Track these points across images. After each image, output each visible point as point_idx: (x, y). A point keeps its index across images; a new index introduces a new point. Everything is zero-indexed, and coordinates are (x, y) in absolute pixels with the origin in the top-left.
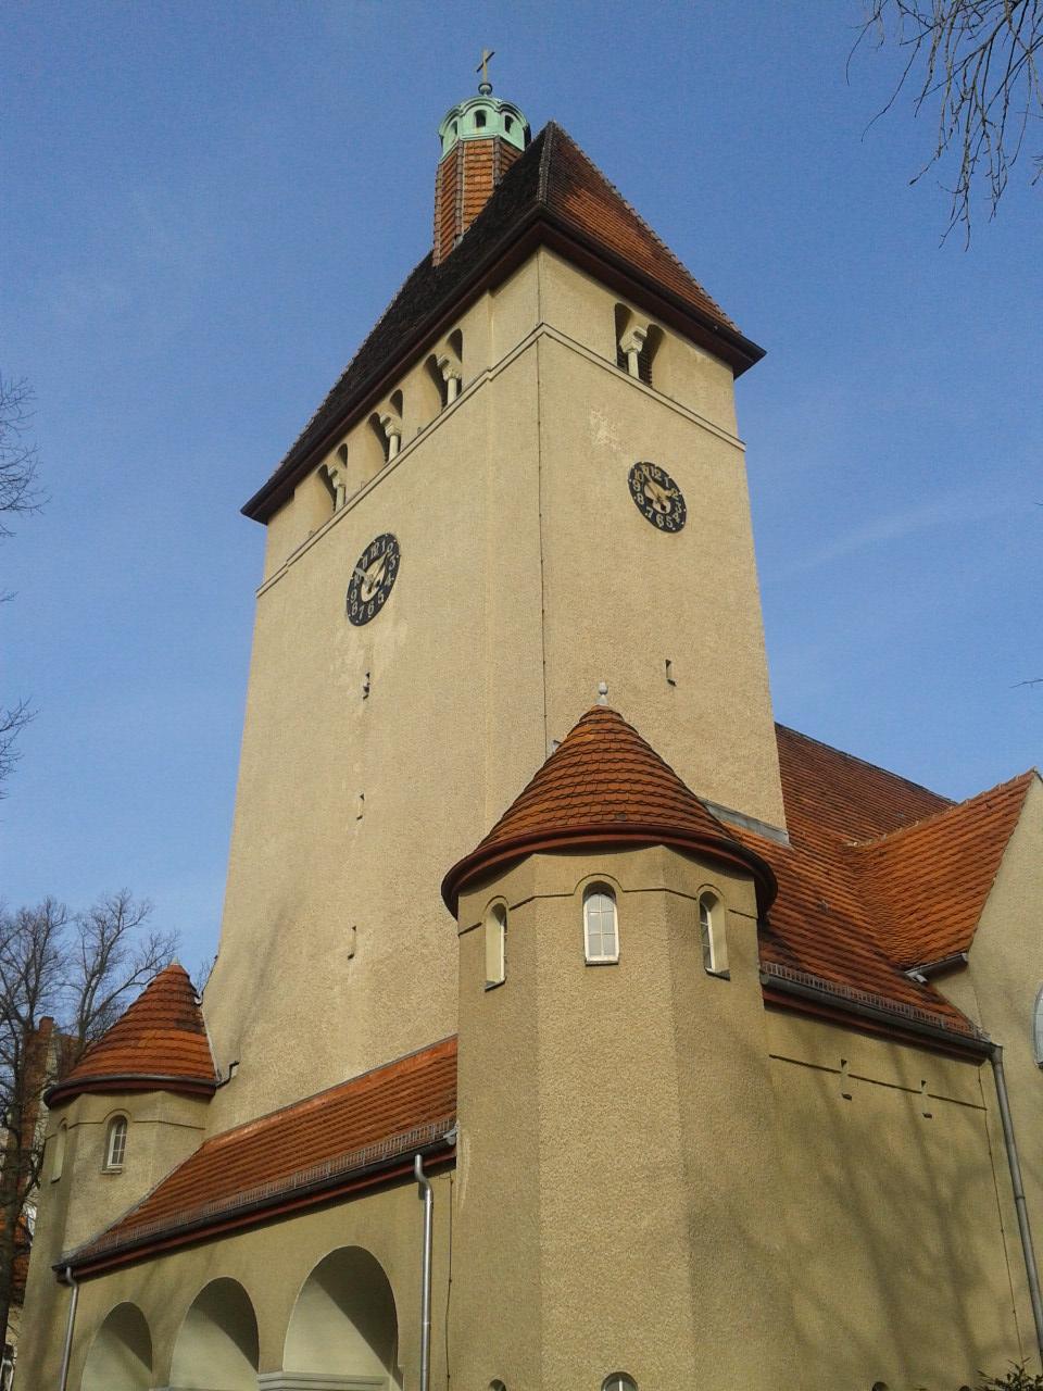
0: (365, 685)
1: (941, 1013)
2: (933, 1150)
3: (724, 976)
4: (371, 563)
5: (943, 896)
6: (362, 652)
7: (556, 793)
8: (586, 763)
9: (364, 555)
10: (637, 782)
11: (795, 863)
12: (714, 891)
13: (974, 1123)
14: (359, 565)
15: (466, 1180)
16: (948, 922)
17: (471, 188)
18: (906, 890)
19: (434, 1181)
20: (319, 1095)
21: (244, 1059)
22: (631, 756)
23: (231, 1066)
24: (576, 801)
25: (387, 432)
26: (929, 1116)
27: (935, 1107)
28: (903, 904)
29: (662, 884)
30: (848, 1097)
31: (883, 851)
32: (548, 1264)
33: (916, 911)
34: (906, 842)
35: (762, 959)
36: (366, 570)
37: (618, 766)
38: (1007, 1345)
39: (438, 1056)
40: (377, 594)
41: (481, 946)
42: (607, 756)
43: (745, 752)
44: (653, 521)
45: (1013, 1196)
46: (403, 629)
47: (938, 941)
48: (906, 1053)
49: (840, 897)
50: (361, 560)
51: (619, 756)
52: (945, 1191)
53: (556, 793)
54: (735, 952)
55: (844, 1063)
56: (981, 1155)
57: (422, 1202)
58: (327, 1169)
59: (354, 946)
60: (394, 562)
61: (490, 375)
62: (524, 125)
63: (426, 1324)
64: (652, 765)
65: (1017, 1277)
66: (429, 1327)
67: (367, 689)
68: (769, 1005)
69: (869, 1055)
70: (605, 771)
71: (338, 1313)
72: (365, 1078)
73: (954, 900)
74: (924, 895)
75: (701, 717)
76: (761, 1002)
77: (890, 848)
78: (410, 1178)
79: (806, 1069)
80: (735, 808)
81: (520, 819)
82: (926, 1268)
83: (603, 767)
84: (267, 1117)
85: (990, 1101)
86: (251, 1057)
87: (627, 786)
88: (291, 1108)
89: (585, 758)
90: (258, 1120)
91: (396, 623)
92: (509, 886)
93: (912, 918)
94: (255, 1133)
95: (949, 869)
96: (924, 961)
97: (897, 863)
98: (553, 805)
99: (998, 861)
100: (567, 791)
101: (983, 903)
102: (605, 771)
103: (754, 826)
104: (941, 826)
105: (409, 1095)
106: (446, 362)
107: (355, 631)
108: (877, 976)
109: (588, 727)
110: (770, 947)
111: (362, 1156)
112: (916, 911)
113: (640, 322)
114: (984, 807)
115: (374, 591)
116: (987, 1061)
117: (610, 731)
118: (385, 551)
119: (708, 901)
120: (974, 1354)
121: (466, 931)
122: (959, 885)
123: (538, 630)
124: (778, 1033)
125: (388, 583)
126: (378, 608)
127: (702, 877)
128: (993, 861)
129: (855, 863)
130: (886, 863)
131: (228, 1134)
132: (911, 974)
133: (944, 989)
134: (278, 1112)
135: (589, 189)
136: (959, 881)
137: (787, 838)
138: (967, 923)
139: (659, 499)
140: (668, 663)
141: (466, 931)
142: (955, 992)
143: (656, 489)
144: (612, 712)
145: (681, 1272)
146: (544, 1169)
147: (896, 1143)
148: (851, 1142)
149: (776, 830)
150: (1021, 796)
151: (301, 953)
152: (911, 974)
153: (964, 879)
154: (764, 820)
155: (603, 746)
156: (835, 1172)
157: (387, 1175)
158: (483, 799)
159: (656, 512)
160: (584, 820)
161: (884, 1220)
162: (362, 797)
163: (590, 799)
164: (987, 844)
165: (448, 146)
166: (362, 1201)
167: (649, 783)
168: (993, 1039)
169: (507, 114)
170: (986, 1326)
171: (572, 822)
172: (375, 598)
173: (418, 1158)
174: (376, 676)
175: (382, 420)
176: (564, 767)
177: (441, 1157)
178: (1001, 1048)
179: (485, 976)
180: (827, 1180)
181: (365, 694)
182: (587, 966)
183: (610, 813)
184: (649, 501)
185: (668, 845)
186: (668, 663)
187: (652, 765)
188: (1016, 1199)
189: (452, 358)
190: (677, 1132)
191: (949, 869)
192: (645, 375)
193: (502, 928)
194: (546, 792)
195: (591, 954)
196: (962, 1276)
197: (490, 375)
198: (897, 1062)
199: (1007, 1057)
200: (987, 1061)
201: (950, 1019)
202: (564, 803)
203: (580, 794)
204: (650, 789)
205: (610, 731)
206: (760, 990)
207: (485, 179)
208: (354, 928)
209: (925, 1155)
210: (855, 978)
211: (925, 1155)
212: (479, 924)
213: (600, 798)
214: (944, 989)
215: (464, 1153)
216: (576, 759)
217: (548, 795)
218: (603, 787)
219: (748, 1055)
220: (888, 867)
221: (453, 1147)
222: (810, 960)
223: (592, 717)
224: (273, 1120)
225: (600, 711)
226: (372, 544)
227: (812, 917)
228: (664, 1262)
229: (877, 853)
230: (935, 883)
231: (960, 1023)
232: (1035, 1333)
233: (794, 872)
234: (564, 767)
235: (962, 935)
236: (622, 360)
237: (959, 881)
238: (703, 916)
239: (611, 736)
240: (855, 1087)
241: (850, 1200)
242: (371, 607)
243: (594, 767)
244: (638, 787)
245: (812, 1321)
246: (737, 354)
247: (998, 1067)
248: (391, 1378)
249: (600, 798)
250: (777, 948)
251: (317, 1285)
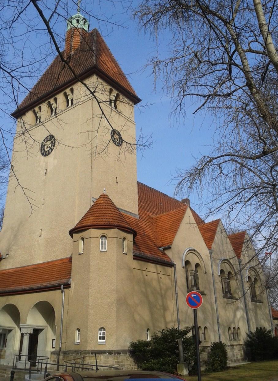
0: (46, 172)
1: (165, 257)
2: (161, 284)
3: (126, 254)
4: (47, 141)
5: (168, 232)
6: (45, 163)
7: (96, 215)
8: (101, 208)
9: (46, 138)
10: (112, 214)
11: (140, 223)
12: (126, 237)
13: (169, 279)
14: (44, 140)
15: (73, 291)
16: (169, 238)
17: (75, 41)
18: (161, 229)
19: (65, 290)
20: (31, 265)
21: (9, 254)
22: (110, 207)
23: (6, 255)
24: (100, 217)
25: (52, 107)
26: (161, 278)
27: (163, 276)
28: (160, 232)
29: (116, 236)
30: (147, 275)
31: (157, 219)
32: (90, 308)
33: (162, 234)
34: (162, 217)
35: (133, 249)
36: (46, 142)
37: (108, 210)
38: (172, 321)
39: (62, 262)
40: (49, 150)
41: (78, 244)
42: (106, 207)
43: (131, 198)
44: (115, 144)
45: (175, 293)
46: (56, 161)
47: (166, 242)
48: (158, 266)
49: (149, 232)
50: (45, 139)
51: (108, 207)
52: (163, 292)
53: (96, 215)
54: (129, 249)
55: (146, 269)
56: (170, 285)
57: (62, 294)
58: (40, 285)
59: (41, 234)
60: (54, 143)
61: (81, 103)
62: (88, 24)
63: (62, 317)
64: (115, 209)
65: (175, 308)
66: (63, 318)
67: (46, 173)
68: (134, 259)
69: (151, 267)
70: (105, 211)
71: (39, 313)
72: (43, 264)
73: (170, 233)
74: (164, 231)
75: (123, 190)
76: (133, 258)
77: (159, 218)
78: (60, 289)
79: (139, 270)
80: (128, 211)
81: (88, 220)
82: (158, 307)
83: (105, 210)
84: (16, 268)
85: (173, 275)
86: (12, 253)
87: (110, 215)
88: (23, 267)
89: (101, 207)
90: (13, 268)
91: (54, 159)
92: (85, 234)
93: (162, 236)
94: (13, 271)
95: (170, 226)
96: (163, 246)
97: (160, 222)
98: (95, 218)
99: (179, 226)
100: (98, 215)
101: (175, 235)
102: (105, 211)
103: (132, 214)
104: (169, 215)
105: (56, 270)
106: (69, 95)
107: (43, 157)
108: (154, 250)
109: (102, 199)
110: (135, 246)
111: (48, 284)
112: (162, 234)
113: (115, 93)
114: (178, 212)
115: (48, 149)
116: (173, 267)
117: (106, 200)
118: (51, 138)
119: (124, 239)
120: (166, 323)
121: (75, 242)
122: (171, 230)
123: (90, 171)
124: (135, 264)
125: (52, 148)
126: (49, 154)
127: (123, 234)
128: (178, 226)
129: (152, 221)
130: (158, 222)
131: (5, 270)
132: (160, 249)
133: (166, 252)
134: (19, 267)
135: (105, 53)
136: (171, 229)
137: (138, 217)
138: (172, 239)
139: (117, 138)
140: (117, 178)
141: (75, 242)
142: (168, 253)
143: (116, 136)
144: (106, 195)
145: (115, 309)
146: (90, 290)
147: (155, 284)
148: (146, 283)
149: (136, 215)
150: (185, 211)
151: (26, 232)
152: (160, 249)
153: (172, 229)
154: (134, 213)
155: (105, 204)
156: (144, 290)
157: (56, 288)
158: (75, 207)
159: (116, 142)
160: (102, 222)
161: (151, 298)
162: (44, 199)
163: (102, 217)
164: (177, 221)
165: (69, 28)
166: (49, 292)
167: (114, 214)
168: (175, 263)
169: (85, 21)
170: (169, 318)
171: (99, 223)
172: (49, 151)
173: (62, 286)
174: (48, 171)
175: (51, 103)
176: (97, 208)
177: (67, 286)
178: (176, 264)
179: (79, 251)
180: (142, 291)
181: (45, 174)
182: (101, 252)
183: (107, 221)
184: (115, 139)
185: (117, 228)
186: (117, 178)
187: (115, 209)
188: (176, 294)
189: (71, 94)
190: (116, 284)
191: (170, 226)
192: (115, 106)
193: (83, 242)
194: (93, 214)
195: (101, 249)
196: (165, 308)
197: (81, 103)
198: (156, 268)
199: (177, 266)
200: (173, 267)
201: (167, 259)
202: (97, 218)
203: (100, 216)
204: (114, 215)
205: (106, 200)
206: (132, 256)
207: (78, 39)
208: (41, 230)
209: (160, 285)
210: (150, 251)
211: (160, 285)
212: (78, 241)
213: (104, 217)
214: (166, 252)
215: (73, 286)
216: (99, 207)
217: (93, 215)
218: (105, 215)
219: (130, 270)
220: (158, 223)
221: (70, 284)
222: (142, 248)
223: (103, 196)
224: (18, 269)
225: (104, 195)
226: (48, 136)
227: (143, 237)
228: (112, 308)
229: (156, 219)
230: (167, 228)
231: (168, 259)
232: (177, 319)
233: (140, 226)
234: (97, 208)
235: (171, 241)
236: (110, 101)
237: (171, 229)
238: (123, 241)
239: (106, 202)
240: (148, 274)
241: (146, 296)
242: (47, 153)
243: (103, 210)
244: (112, 215)
245: (137, 317)
246: (135, 100)
247: (175, 268)
248: (48, 326)
249: (104, 217)
250: (136, 246)
251: (35, 308)
